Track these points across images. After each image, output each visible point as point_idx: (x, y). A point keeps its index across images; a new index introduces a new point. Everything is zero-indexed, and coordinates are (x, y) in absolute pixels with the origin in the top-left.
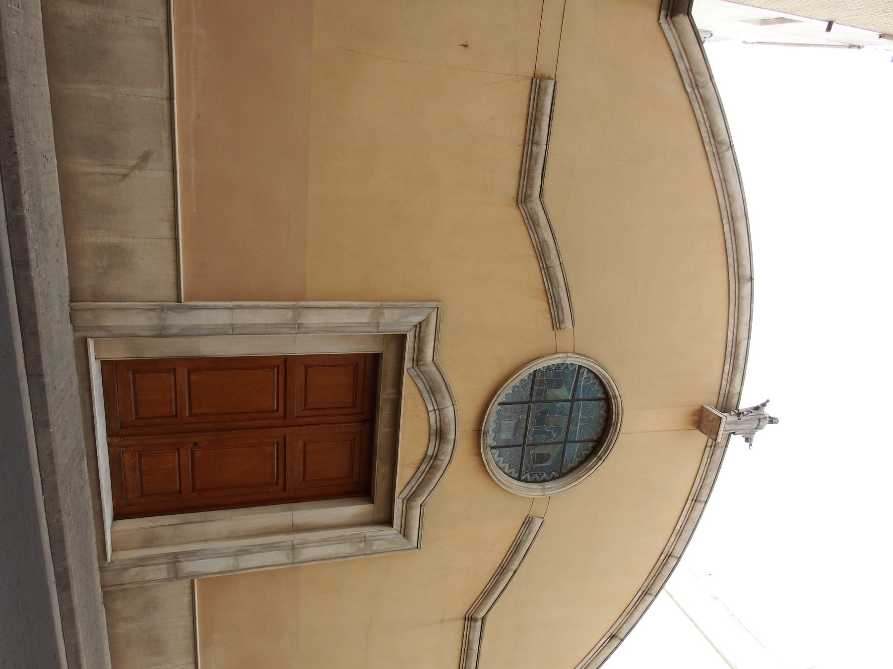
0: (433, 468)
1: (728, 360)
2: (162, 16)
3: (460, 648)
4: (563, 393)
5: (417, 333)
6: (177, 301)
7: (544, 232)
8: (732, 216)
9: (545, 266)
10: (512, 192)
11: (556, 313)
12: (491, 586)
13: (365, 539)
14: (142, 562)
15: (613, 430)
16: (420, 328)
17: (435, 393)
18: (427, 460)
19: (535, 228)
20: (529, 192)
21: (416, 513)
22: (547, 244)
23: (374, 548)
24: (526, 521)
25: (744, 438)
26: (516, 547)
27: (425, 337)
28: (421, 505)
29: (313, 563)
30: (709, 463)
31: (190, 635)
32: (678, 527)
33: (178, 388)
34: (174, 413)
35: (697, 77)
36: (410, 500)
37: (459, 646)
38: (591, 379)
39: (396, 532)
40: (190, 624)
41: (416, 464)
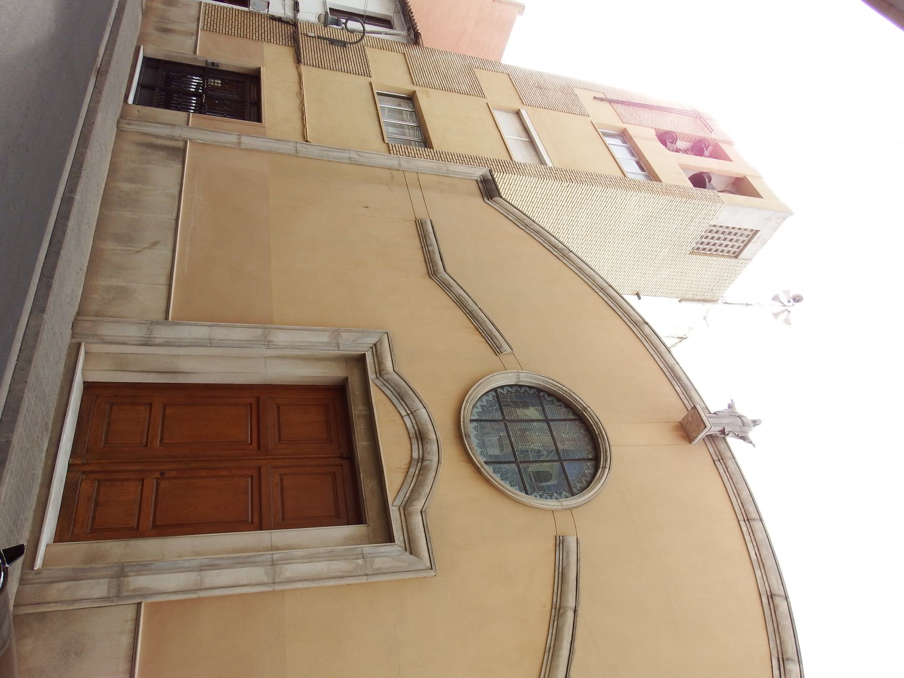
1: (674, 382)
5: (374, 352)
7: (457, 290)
10: (424, 270)
12: (553, 638)
15: (601, 440)
16: (375, 348)
17: (403, 398)
19: (449, 289)
20: (435, 269)
21: (417, 520)
23: (376, 566)
24: (558, 542)
26: (560, 576)
28: (421, 511)
30: (731, 478)
34: (145, 444)
35: (524, 221)
38: (580, 484)
39: (399, 548)
41: (404, 469)
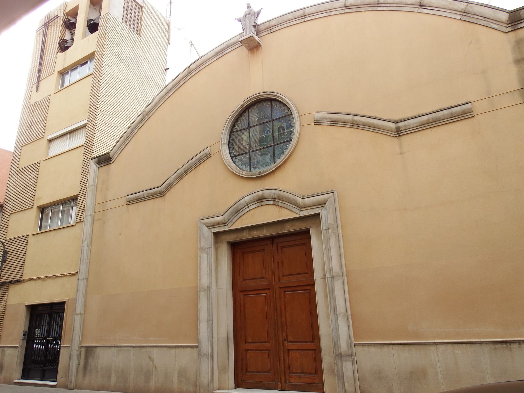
0: (280, 198)
1: (225, 53)
2: (113, 349)
3: (430, 130)
5: (212, 227)
8: (167, 94)
9: (185, 173)
10: (160, 199)
11: (204, 159)
18: (276, 203)
19: (171, 184)
20: (159, 192)
21: (308, 201)
22: (176, 176)
23: (332, 222)
24: (318, 124)
27: (212, 223)
28: (303, 199)
30: (280, 24)
31: (406, 348)
33: (255, 349)
34: (268, 351)
39: (323, 211)
40: (396, 347)
41: (279, 208)
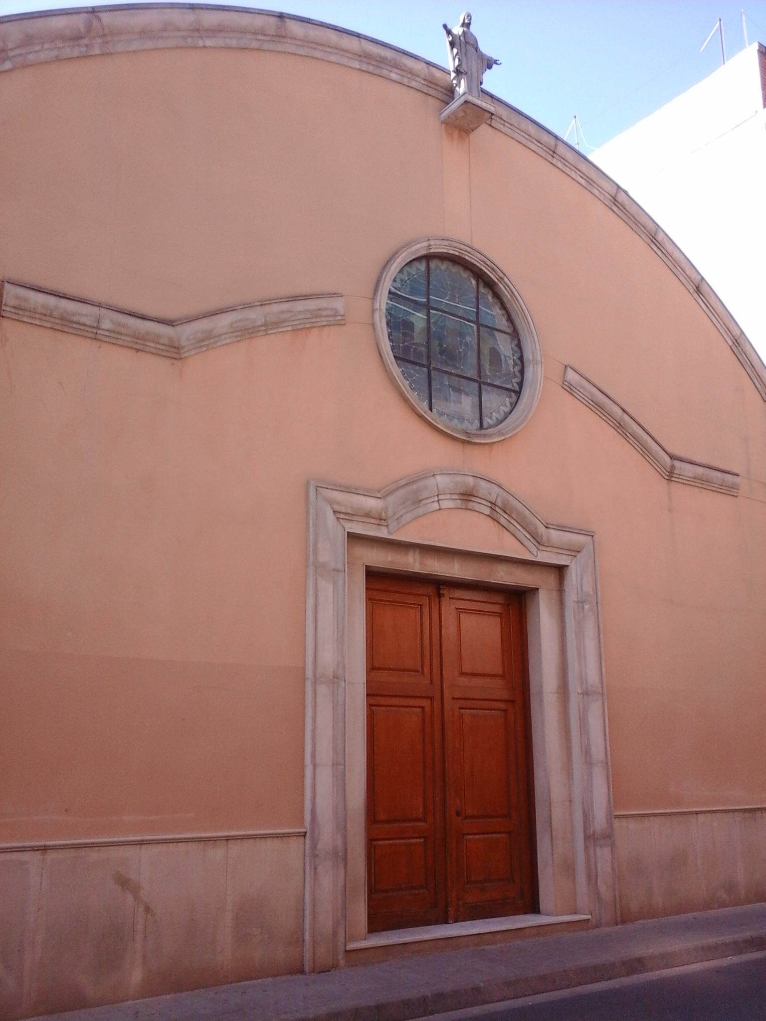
4: (419, 319)
6: (303, 838)
13: (581, 602)
14: (592, 877)
20: (166, 341)
24: (568, 389)
25: (487, 70)
26: (598, 408)
28: (546, 527)
29: (604, 669)
30: (511, 125)
32: (583, 182)
36: (539, 541)
37: (697, 490)
